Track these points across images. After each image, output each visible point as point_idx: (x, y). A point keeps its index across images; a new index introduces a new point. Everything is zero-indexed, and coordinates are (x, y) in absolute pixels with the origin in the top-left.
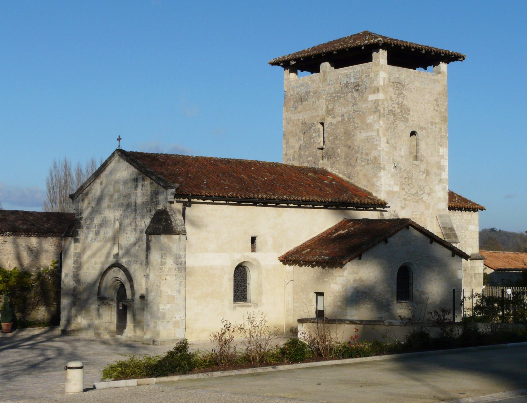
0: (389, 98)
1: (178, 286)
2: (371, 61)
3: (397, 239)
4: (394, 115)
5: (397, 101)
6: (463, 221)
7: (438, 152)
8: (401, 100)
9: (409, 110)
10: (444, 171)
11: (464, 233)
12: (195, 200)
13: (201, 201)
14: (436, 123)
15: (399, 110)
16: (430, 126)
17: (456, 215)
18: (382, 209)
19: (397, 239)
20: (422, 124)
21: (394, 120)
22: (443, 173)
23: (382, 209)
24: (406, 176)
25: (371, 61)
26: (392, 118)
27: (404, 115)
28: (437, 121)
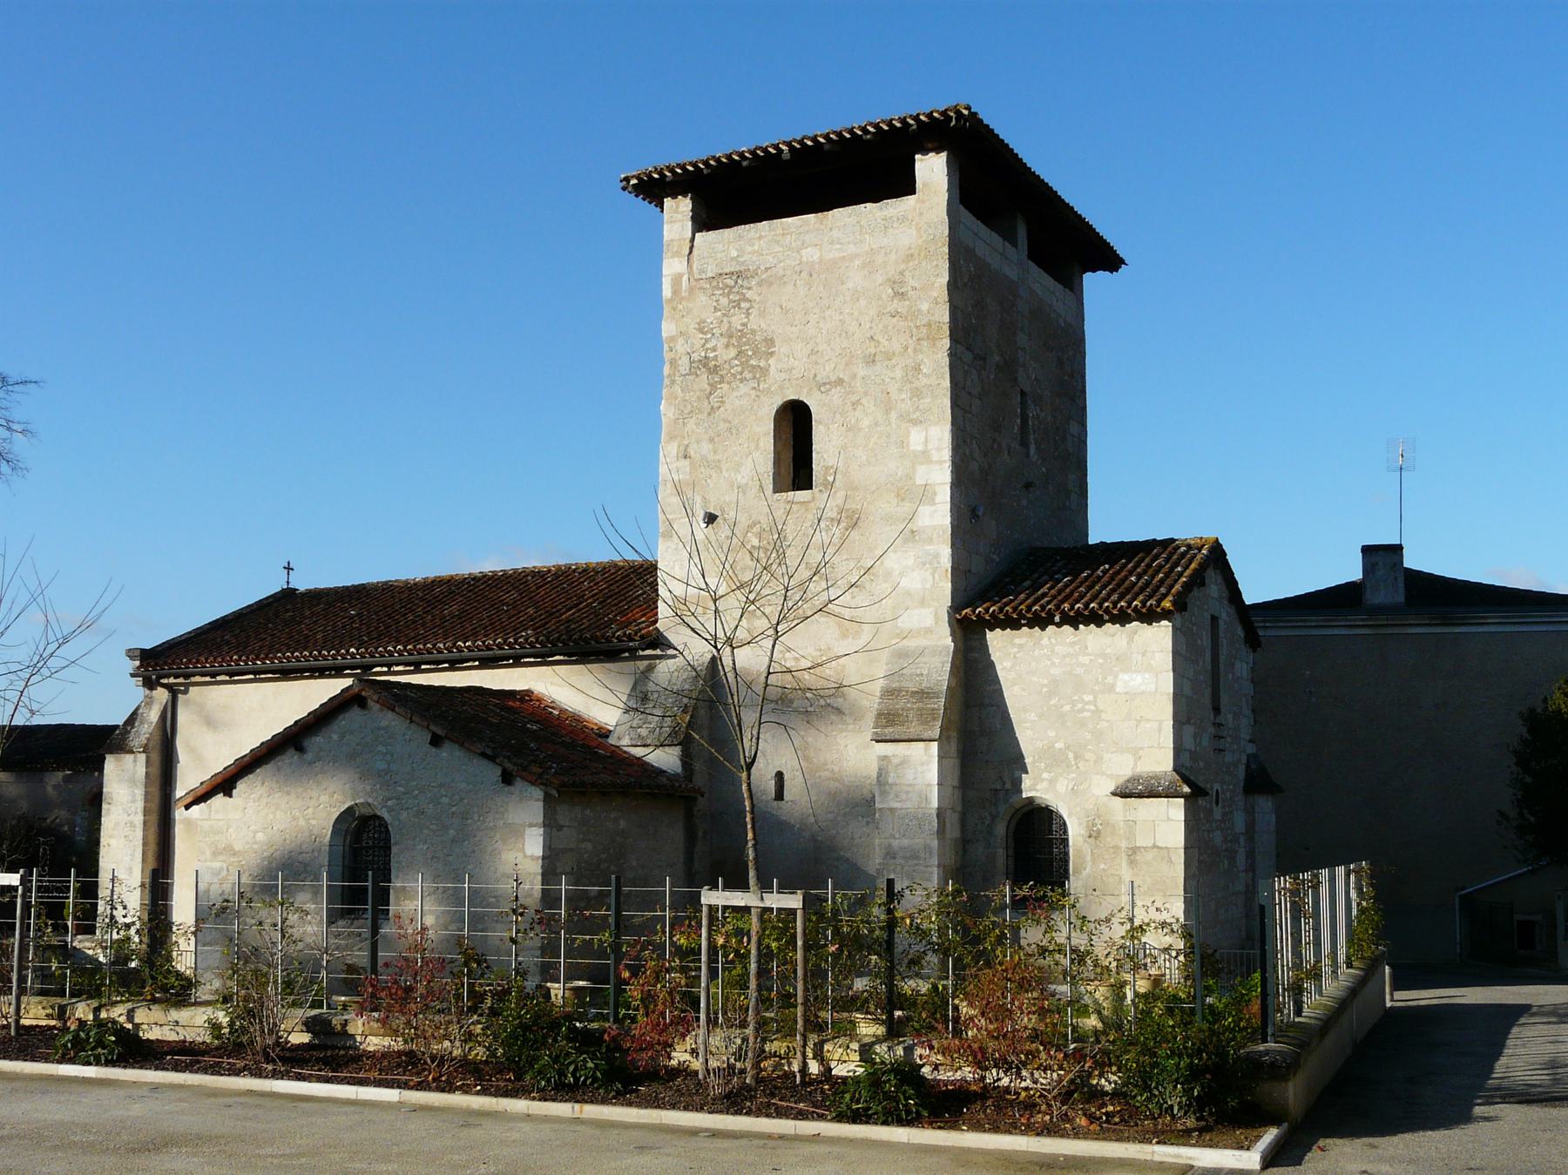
0: (693, 325)
1: (127, 859)
2: (913, 192)
3: (335, 737)
4: (714, 370)
5: (724, 330)
6: (1085, 660)
7: (903, 444)
8: (737, 320)
9: (770, 342)
10: (932, 502)
11: (1094, 703)
12: (198, 679)
13: (208, 679)
14: (889, 356)
15: (733, 352)
16: (862, 371)
17: (1045, 641)
18: (658, 652)
19: (335, 737)
20: (826, 372)
21: (713, 386)
22: (925, 510)
23: (658, 652)
24: (755, 542)
25: (913, 192)
26: (703, 380)
27: (753, 362)
28: (896, 346)
